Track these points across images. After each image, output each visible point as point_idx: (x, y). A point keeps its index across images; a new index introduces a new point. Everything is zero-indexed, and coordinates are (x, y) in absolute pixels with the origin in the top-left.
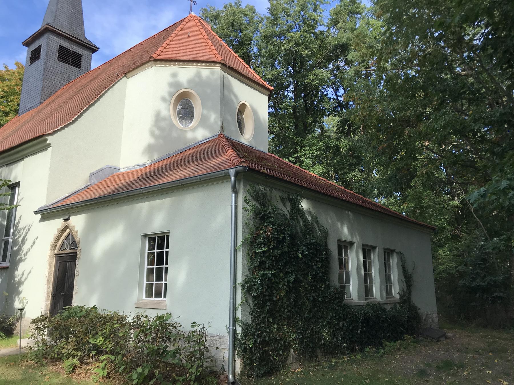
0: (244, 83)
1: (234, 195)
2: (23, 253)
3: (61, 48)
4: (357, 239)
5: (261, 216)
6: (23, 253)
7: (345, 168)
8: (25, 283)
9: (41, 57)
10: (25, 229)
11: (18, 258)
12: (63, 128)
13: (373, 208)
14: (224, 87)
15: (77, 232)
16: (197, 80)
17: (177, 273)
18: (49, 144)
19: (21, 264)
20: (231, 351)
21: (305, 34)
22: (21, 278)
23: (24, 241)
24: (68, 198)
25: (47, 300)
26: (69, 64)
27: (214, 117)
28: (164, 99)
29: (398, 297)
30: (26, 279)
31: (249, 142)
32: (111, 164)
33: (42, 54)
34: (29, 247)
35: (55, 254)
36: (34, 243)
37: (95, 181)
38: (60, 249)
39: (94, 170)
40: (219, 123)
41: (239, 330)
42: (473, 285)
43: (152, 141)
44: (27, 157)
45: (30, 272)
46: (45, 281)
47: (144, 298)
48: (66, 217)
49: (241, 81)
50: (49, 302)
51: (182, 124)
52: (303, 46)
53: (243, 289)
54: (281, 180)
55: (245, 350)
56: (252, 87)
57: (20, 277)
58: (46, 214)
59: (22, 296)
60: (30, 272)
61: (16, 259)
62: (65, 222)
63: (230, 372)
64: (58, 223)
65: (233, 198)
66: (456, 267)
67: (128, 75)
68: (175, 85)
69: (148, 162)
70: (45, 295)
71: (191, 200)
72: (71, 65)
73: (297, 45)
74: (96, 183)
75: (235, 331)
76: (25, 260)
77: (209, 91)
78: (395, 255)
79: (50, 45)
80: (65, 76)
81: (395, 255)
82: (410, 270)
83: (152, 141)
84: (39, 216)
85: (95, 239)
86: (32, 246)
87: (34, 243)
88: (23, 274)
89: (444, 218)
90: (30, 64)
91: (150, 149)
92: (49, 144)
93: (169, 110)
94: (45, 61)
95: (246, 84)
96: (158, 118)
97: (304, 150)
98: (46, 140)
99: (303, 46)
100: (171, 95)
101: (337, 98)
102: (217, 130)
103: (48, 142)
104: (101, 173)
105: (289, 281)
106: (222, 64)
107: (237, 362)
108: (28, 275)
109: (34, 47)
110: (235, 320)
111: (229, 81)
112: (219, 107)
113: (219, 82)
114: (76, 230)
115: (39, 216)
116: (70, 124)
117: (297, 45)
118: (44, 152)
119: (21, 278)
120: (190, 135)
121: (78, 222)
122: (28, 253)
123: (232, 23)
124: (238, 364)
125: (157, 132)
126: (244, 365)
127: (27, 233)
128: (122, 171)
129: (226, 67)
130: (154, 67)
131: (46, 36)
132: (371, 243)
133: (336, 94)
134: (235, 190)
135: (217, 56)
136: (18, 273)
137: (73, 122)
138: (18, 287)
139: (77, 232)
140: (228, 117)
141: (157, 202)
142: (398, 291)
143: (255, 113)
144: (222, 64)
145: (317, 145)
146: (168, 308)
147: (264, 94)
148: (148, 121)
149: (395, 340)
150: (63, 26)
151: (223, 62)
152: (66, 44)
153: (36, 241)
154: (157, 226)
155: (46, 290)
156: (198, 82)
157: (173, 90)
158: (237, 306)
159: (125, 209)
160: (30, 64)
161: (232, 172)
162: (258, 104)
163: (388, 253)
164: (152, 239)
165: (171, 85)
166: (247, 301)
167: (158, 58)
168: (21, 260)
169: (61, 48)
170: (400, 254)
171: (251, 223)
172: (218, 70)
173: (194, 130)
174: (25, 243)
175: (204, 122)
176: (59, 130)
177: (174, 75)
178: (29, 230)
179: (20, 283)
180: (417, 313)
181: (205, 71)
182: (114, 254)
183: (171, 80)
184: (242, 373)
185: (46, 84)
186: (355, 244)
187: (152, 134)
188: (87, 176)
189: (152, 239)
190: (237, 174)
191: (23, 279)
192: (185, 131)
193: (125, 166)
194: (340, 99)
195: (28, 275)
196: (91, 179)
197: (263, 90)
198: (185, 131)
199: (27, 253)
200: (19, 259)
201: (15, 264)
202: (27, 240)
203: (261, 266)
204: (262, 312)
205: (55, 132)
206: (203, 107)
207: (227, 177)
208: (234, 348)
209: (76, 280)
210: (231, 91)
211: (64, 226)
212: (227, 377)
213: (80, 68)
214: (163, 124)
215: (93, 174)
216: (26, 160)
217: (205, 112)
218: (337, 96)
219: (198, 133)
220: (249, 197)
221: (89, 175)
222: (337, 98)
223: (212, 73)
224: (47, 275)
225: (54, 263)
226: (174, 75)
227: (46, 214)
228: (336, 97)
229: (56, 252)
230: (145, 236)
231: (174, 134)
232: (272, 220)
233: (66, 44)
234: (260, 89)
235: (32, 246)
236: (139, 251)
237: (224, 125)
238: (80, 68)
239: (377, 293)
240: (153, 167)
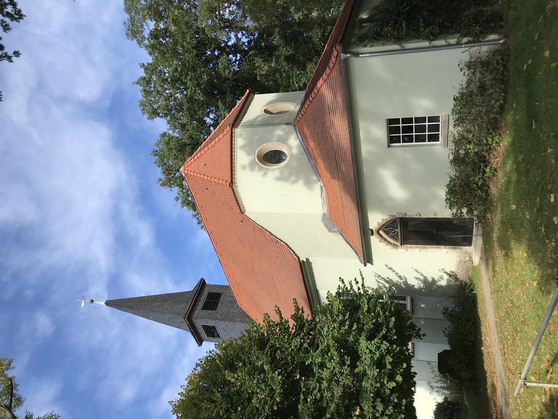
1: (360, 56)
2: (399, 280)
3: (204, 308)
5: (377, 37)
6: (399, 280)
7: (308, 48)
8: (425, 275)
9: (213, 325)
10: (379, 280)
11: (404, 286)
12: (293, 251)
14: (251, 125)
15: (383, 220)
16: (247, 148)
17: (422, 107)
18: (306, 259)
19: (409, 283)
20: (482, 44)
21: (188, 78)
22: (421, 280)
23: (389, 281)
24: (352, 245)
25: (441, 248)
26: (218, 302)
27: (279, 132)
28: (265, 175)
30: (422, 275)
31: (298, 105)
32: (320, 218)
33: (210, 323)
34: (394, 274)
36: (390, 269)
37: (335, 229)
39: (326, 230)
40: (284, 126)
41: (465, 40)
43: (301, 182)
44: (315, 286)
45: (416, 270)
46: (424, 250)
48: (370, 232)
49: (245, 114)
51: (284, 160)
53: (433, 40)
55: (481, 32)
57: (420, 282)
58: (367, 258)
59: (436, 279)
60: (416, 270)
62: (374, 234)
63: (498, 42)
64: (374, 240)
65: (363, 55)
67: (243, 211)
68: (252, 165)
69: (319, 183)
70: (436, 250)
72: (219, 300)
73: (198, 85)
76: (405, 278)
77: (256, 137)
83: (301, 182)
85: (391, 199)
86: (394, 271)
87: (390, 269)
88: (417, 278)
90: (219, 337)
91: (308, 184)
92: (306, 259)
93: (274, 169)
95: (247, 110)
97: (293, 83)
98: (303, 261)
100: (261, 169)
101: (237, 60)
102: (290, 128)
103: (305, 260)
105: (428, 15)
106: (233, 127)
111: (246, 122)
112: (270, 128)
113: (248, 129)
114: (381, 221)
116: (288, 246)
118: (313, 266)
119: (421, 280)
120: (295, 151)
121: (375, 220)
122: (400, 275)
123: (179, 151)
124: (493, 37)
125: (293, 178)
126: (493, 32)
127: (382, 278)
129: (235, 123)
130: (237, 184)
131: (194, 321)
133: (233, 62)
134: (357, 55)
135: (225, 132)
137: (286, 244)
138: (429, 282)
139: (383, 220)
140: (277, 121)
141: (362, 135)
143: (270, 103)
144: (233, 127)
145: (288, 71)
146: (447, 113)
148: (284, 186)
150: (185, 308)
151: (231, 126)
152: (201, 304)
153: (389, 266)
154: (380, 132)
155: (432, 249)
156: (249, 147)
157: (257, 168)
159: (366, 169)
160: (219, 337)
161: (343, 56)
164: (392, 140)
165: (252, 169)
166: (444, 37)
167: (230, 181)
168: (406, 283)
169: (204, 308)
171: (382, 42)
172: (238, 131)
173: (290, 148)
174: (391, 280)
175: (283, 140)
176: (294, 253)
177: (244, 167)
178: (379, 276)
179: (425, 281)
181: (239, 142)
182: (404, 179)
183: (248, 170)
184: (499, 33)
187: (295, 182)
188: (332, 234)
190: (345, 52)
191: (422, 278)
192: (292, 155)
194: (238, 58)
196: (334, 232)
197: (250, 98)
198: (292, 155)
199: (400, 276)
201: (409, 289)
202: (388, 278)
203: (417, 30)
205: (296, 255)
206: (270, 141)
207: (346, 61)
208: (480, 42)
209: (423, 216)
211: (377, 235)
212: (502, 44)
213: (221, 294)
214: (286, 174)
216: (318, 287)
217: (274, 139)
218: (236, 60)
219: (292, 145)
220: (363, 44)
221: (331, 234)
222: (237, 60)
223: (241, 135)
225: (408, 246)
226: (244, 167)
227: (367, 258)
228: (237, 62)
229: (399, 244)
230: (389, 146)
231: (295, 164)
233: (201, 304)
234: (246, 106)
235: (394, 271)
236: (402, 150)
238: (221, 294)
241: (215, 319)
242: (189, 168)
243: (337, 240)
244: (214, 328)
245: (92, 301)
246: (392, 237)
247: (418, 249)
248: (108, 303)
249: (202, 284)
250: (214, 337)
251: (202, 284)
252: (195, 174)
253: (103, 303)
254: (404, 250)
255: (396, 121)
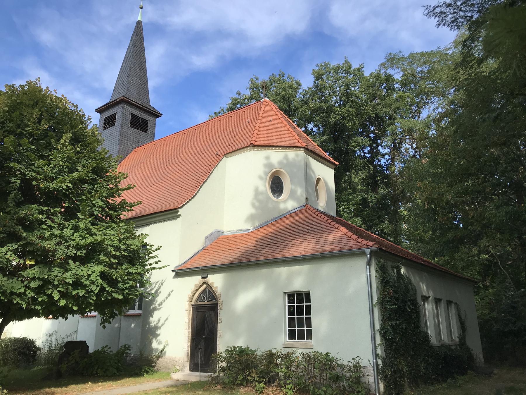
0: (318, 161)
1: (368, 267)
2: (158, 303)
3: (133, 116)
4: (431, 294)
5: (384, 283)
6: (158, 303)
7: (374, 220)
8: (162, 328)
10: (158, 284)
11: (152, 307)
13: (431, 265)
14: (307, 165)
15: (216, 288)
16: (285, 162)
17: (320, 322)
19: (155, 312)
23: (157, 293)
25: (188, 342)
26: (138, 129)
27: (300, 191)
28: (261, 178)
29: (457, 340)
30: (162, 325)
33: (118, 121)
34: (164, 298)
35: (192, 305)
36: (169, 295)
37: (208, 243)
38: (197, 300)
40: (305, 196)
41: (380, 362)
42: (506, 330)
43: (253, 211)
45: (167, 319)
47: (288, 340)
48: (205, 276)
49: (316, 160)
50: (189, 344)
52: (348, 119)
53: (380, 334)
54: (391, 253)
55: (386, 376)
56: (323, 164)
57: (155, 323)
58: (180, 273)
60: (167, 319)
61: (150, 307)
64: (197, 280)
65: (368, 269)
66: (489, 314)
67: (227, 155)
68: (269, 165)
69: (252, 228)
70: (187, 338)
71: (328, 269)
73: (343, 118)
74: (209, 245)
75: (377, 363)
78: (453, 305)
79: (122, 113)
80: (135, 140)
81: (453, 305)
82: (463, 317)
83: (253, 211)
84: (174, 273)
86: (167, 298)
87: (169, 295)
88: (159, 320)
89: (475, 269)
91: (251, 218)
93: (266, 186)
94: (120, 127)
96: (257, 192)
98: (178, 212)
99: (348, 119)
100: (266, 174)
101: (364, 155)
102: (303, 202)
103: (179, 214)
104: (212, 236)
107: (380, 385)
108: (165, 321)
109: (107, 114)
110: (376, 356)
112: (304, 183)
114: (215, 286)
115: (174, 273)
116: (192, 198)
117: (343, 118)
118: (173, 221)
119: (157, 324)
120: (282, 206)
121: (216, 281)
122: (163, 304)
123: (284, 97)
124: (382, 387)
125: (257, 204)
127: (160, 287)
128: (225, 234)
129: (309, 151)
132: (439, 297)
134: (369, 264)
135: (300, 141)
136: (154, 320)
138: (155, 331)
139: (216, 288)
140: (310, 190)
142: (457, 335)
143: (326, 184)
145: (354, 200)
147: (331, 168)
148: (250, 195)
149: (463, 374)
150: (134, 97)
151: (306, 147)
152: (136, 112)
153: (171, 294)
154: (297, 286)
155: (187, 335)
156: (287, 164)
158: (377, 345)
159: (264, 271)
160: (104, 130)
161: (368, 251)
162: (327, 174)
163: (449, 303)
164: (291, 296)
165: (266, 166)
168: (155, 309)
169: (133, 116)
170: (456, 304)
171: (380, 287)
172: (301, 153)
173: (285, 201)
175: (292, 195)
176: (186, 204)
177: (268, 158)
178: (162, 284)
180: (471, 353)
181: (291, 154)
183: (265, 162)
184: (385, 392)
185: (121, 148)
186: (431, 298)
187: (253, 205)
188: (203, 239)
189: (291, 296)
190: (371, 253)
191: (160, 325)
193: (229, 230)
194: (366, 155)
195: (165, 321)
196: (206, 242)
197: (331, 165)
199: (161, 303)
200: (153, 308)
201: (149, 313)
202: (160, 292)
203: (389, 318)
204: (391, 350)
205: (184, 205)
206: (292, 182)
207: (363, 254)
209: (219, 326)
210: (310, 168)
211: (202, 282)
213: (146, 132)
214: (261, 197)
215: (207, 237)
217: (293, 187)
218: (365, 153)
219: (288, 203)
220: (378, 269)
221: (204, 239)
222: (364, 155)
223: (297, 156)
224: (187, 322)
226: (268, 158)
227: (180, 273)
228: (363, 154)
229: (193, 303)
230: (285, 293)
231: (270, 205)
232: (391, 284)
233: (136, 112)
235: (167, 298)
237: (308, 198)
238: (146, 132)
239: (444, 337)
240: (261, 234)
241: (122, 126)
242: (268, 106)
243: (197, 245)
244: (113, 124)
245: (141, 8)
246: (200, 296)
247: (187, 321)
248: (139, 23)
249: (156, 115)
250: (104, 124)
251: (156, 115)
252: (262, 112)
253: (139, 18)
254: (187, 308)
255: (308, 300)
